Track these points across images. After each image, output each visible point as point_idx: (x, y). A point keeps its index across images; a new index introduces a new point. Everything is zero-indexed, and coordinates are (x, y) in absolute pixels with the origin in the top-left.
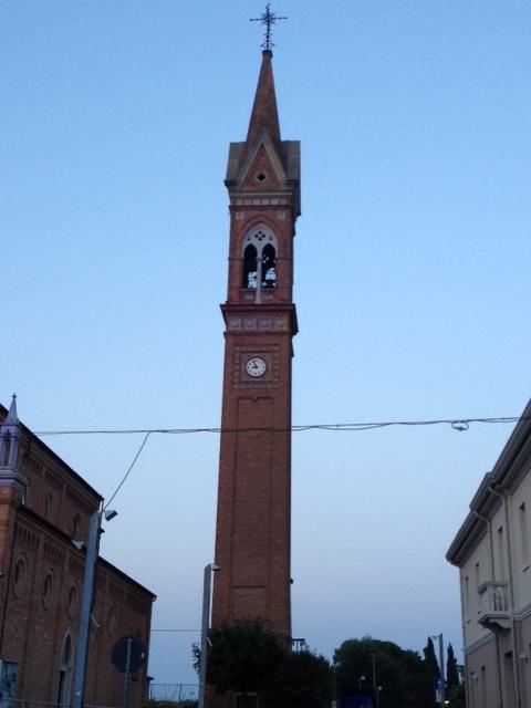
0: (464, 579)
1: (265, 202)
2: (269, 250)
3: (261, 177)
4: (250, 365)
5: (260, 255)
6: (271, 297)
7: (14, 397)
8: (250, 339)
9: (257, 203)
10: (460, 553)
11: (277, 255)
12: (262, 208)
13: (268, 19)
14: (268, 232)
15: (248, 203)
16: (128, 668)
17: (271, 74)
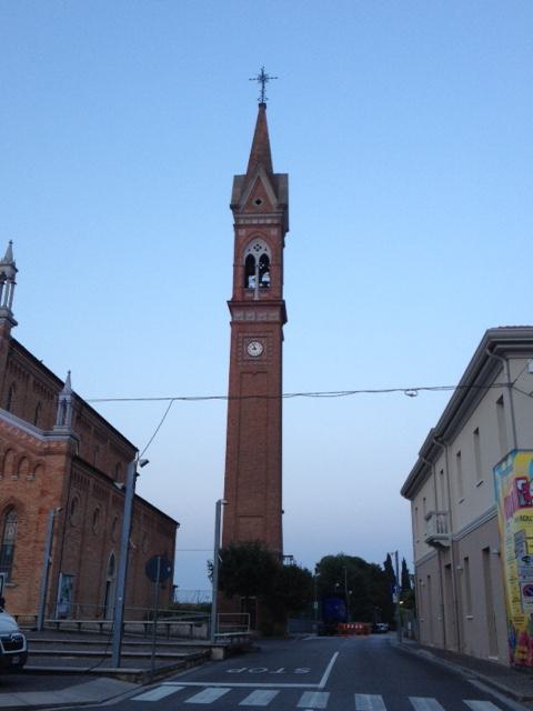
1: (262, 222)
2: (264, 259)
3: (258, 202)
7: (11, 243)
9: (255, 222)
10: (411, 490)
14: (264, 245)
15: (248, 222)
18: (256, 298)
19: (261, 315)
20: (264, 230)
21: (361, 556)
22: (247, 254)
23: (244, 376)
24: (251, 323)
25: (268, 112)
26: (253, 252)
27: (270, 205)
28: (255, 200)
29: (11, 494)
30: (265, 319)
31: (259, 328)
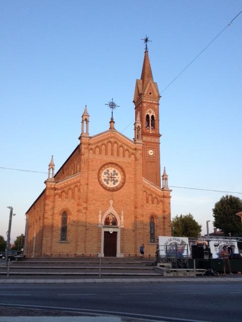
0: (107, 131)
1: (152, 102)
2: (153, 117)
3: (150, 93)
4: (152, 151)
5: (150, 118)
6: (154, 131)
7: (86, 106)
8: (149, 144)
9: (149, 101)
10: (26, 213)
11: (155, 119)
12: (151, 103)
13: (146, 40)
14: (152, 111)
15: (147, 101)
16: (225, 271)
17: (148, 59)
19: (148, 138)
21: (235, 195)
22: (146, 114)
24: (149, 142)
25: (150, 54)
26: (149, 113)
29: (152, 211)
30: (154, 141)
31: (152, 144)
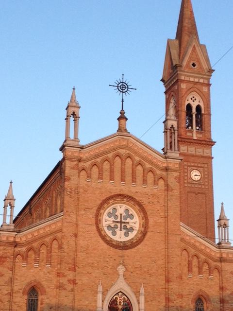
1: (196, 80)
2: (198, 108)
3: (194, 65)
9: (192, 79)
14: (198, 98)
15: (187, 79)
18: (195, 138)
20: (198, 86)
22: (187, 103)
23: (189, 194)
24: (193, 156)
26: (191, 102)
27: (201, 68)
28: (192, 63)
29: (199, 287)
31: (201, 160)
